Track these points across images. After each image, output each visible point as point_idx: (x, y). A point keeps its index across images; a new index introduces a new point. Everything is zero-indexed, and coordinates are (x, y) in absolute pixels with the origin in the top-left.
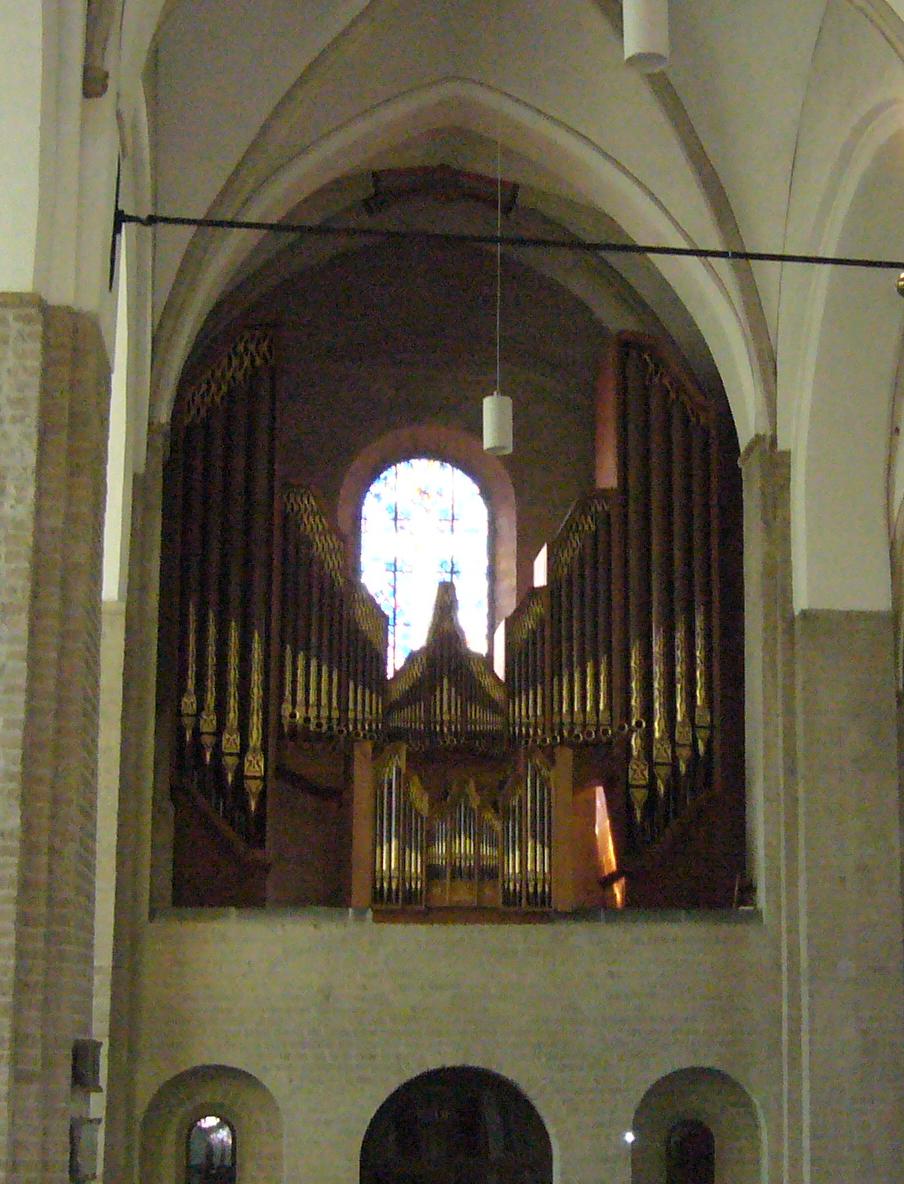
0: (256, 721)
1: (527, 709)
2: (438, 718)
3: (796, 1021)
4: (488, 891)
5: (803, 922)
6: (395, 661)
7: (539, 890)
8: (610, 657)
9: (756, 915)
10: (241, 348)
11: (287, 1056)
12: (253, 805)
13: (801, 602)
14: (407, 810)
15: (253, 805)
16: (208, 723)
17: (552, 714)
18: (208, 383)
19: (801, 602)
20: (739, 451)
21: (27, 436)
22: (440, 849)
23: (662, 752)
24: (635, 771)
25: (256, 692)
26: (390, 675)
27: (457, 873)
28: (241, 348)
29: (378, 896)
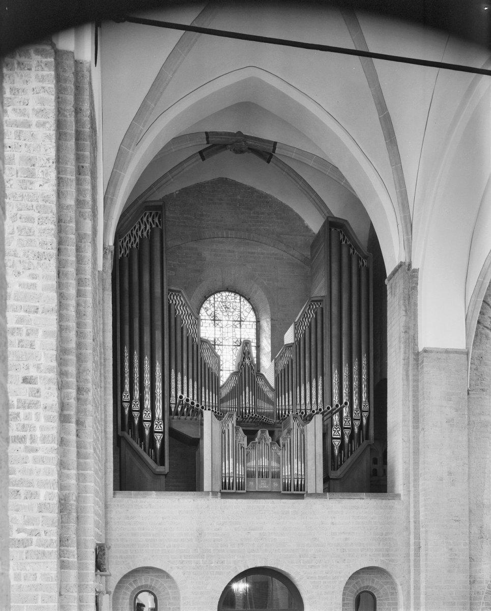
0: (159, 405)
1: (284, 402)
2: (244, 406)
6: (224, 376)
7: (299, 483)
9: (398, 496)
10: (145, 219)
11: (182, 562)
16: (136, 407)
18: (130, 237)
20: (386, 276)
21: (48, 137)
22: (252, 463)
23: (347, 423)
24: (335, 431)
25: (159, 391)
26: (221, 383)
27: (261, 475)
28: (145, 219)
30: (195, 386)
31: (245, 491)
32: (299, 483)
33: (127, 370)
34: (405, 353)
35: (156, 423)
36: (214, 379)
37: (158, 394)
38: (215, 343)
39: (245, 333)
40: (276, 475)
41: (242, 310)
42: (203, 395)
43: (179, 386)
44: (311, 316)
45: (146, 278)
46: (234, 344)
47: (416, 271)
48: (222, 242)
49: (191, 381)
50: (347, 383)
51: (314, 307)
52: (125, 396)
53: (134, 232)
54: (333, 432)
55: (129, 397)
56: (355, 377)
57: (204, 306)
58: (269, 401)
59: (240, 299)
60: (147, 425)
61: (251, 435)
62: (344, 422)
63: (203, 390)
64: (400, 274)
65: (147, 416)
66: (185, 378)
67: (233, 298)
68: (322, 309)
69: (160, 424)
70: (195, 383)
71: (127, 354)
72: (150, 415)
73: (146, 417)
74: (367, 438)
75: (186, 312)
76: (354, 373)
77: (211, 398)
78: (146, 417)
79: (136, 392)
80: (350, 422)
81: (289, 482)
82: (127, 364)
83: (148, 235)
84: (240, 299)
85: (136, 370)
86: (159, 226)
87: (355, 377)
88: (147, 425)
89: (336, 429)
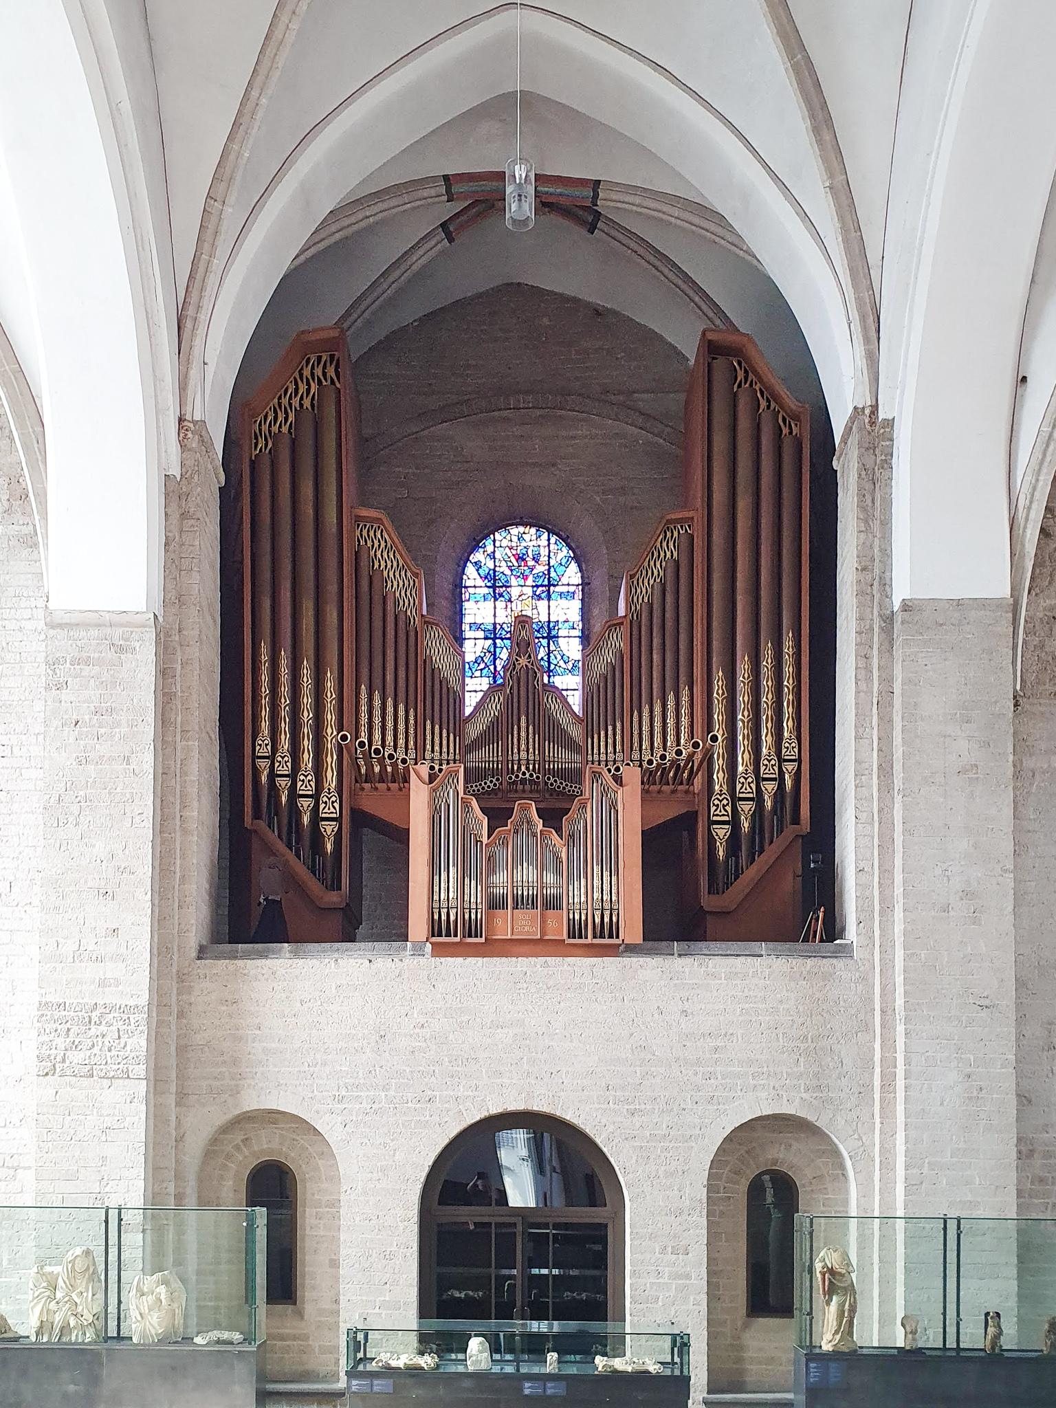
3: (889, 1064)
4: (551, 923)
5: (899, 954)
8: (691, 689)
9: (846, 951)
10: (307, 372)
12: (329, 847)
13: (900, 592)
14: (468, 837)
15: (329, 847)
16: (284, 768)
17: (632, 750)
19: (900, 592)
28: (307, 372)
29: (436, 929)
30: (412, 718)
31: (483, 940)
32: (606, 920)
33: (265, 690)
34: (861, 618)
35: (325, 799)
36: (451, 701)
37: (329, 739)
38: (495, 634)
39: (559, 611)
40: (552, 903)
41: (552, 562)
42: (429, 737)
43: (377, 720)
44: (669, 554)
45: (307, 490)
46: (498, 627)
47: (890, 423)
48: (506, 420)
49: (401, 707)
50: (746, 699)
51: (676, 534)
52: (260, 745)
53: (285, 401)
54: (713, 809)
55: (269, 747)
56: (767, 684)
57: (473, 558)
58: (571, 745)
59: (549, 540)
60: (305, 804)
61: (497, 817)
62: (739, 786)
63: (428, 727)
64: (854, 440)
65: (306, 785)
66: (390, 702)
67: (534, 537)
68: (692, 536)
69: (333, 802)
70: (412, 712)
71: (264, 658)
72: (313, 784)
73: (303, 788)
74: (796, 820)
75: (395, 564)
76: (762, 675)
77: (445, 742)
78: (303, 788)
79: (283, 737)
80: (753, 786)
81: (583, 918)
82: (265, 678)
83: (312, 405)
84: (549, 540)
85: (285, 690)
86: (323, 381)
87: (767, 684)
88: (305, 804)
89: (721, 801)
